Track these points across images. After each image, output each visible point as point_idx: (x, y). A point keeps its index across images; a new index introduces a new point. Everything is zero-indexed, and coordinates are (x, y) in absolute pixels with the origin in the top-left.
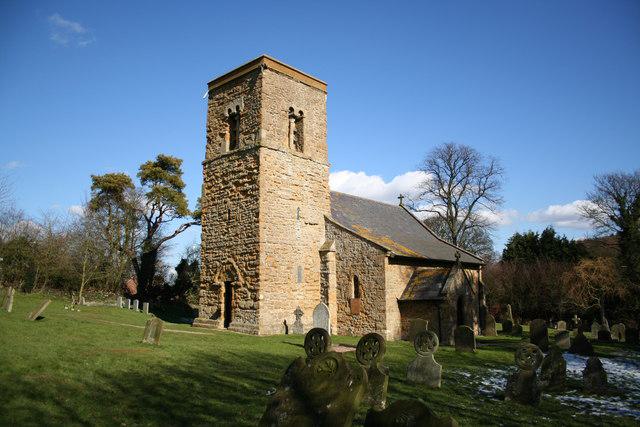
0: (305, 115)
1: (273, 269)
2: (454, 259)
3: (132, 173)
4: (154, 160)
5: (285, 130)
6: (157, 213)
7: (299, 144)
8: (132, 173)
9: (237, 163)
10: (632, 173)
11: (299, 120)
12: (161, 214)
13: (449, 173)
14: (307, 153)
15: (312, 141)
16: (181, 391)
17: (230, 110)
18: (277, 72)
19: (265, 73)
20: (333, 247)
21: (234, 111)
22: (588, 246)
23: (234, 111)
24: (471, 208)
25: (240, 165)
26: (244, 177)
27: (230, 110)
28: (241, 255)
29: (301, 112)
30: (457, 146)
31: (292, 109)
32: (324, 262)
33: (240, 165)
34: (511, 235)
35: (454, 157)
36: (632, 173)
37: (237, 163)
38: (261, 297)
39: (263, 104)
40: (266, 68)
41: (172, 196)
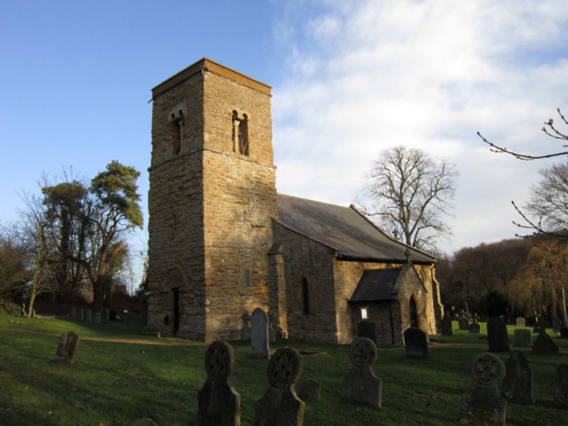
0: (249, 117)
1: (219, 274)
2: (405, 258)
3: (87, 184)
4: (148, 173)
5: (229, 133)
6: (111, 223)
7: (245, 152)
8: (87, 184)
9: (181, 168)
10: (542, 178)
11: (244, 124)
12: (116, 223)
13: (400, 176)
14: (253, 156)
15: (257, 144)
16: (237, 311)
17: (173, 115)
18: (219, 75)
19: (207, 76)
20: (281, 249)
21: (177, 115)
22: (155, 163)
23: (177, 115)
24: (423, 208)
25: (183, 170)
26: (188, 181)
27: (173, 115)
28: (188, 259)
29: (245, 115)
30: (407, 150)
31: (235, 112)
32: (273, 264)
33: (183, 170)
34: (481, 241)
35: (404, 161)
36: (542, 178)
37: (181, 168)
38: (208, 302)
39: (205, 107)
40: (206, 70)
41: (124, 206)
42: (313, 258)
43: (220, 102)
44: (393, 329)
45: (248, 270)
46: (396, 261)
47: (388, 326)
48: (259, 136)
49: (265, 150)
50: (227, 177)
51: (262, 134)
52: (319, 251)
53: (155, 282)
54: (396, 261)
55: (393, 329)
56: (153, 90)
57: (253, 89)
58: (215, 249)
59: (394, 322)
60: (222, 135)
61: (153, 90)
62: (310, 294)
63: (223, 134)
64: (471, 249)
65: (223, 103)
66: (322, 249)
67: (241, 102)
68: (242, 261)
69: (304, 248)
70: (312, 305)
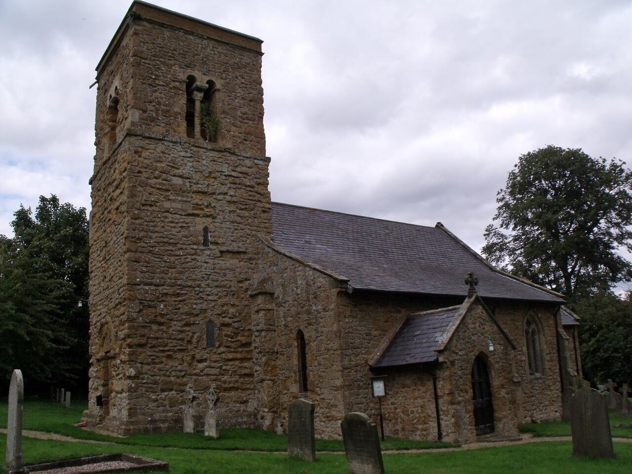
29: (210, 83)
31: (191, 79)
42: (311, 296)
43: (163, 63)
44: (438, 415)
45: (211, 321)
46: (225, 221)
47: (431, 409)
48: (239, 113)
49: (248, 133)
50: (175, 176)
51: (244, 110)
52: (319, 284)
53: (572, 369)
54: (225, 221)
55: (438, 415)
56: (439, 226)
57: (227, 44)
58: (147, 288)
59: (440, 401)
60: (167, 113)
61: (439, 226)
62: (309, 357)
63: (168, 111)
64: (560, 150)
65: (169, 66)
66: (322, 281)
67: (204, 63)
68: (199, 307)
69: (299, 282)
70: (311, 376)
